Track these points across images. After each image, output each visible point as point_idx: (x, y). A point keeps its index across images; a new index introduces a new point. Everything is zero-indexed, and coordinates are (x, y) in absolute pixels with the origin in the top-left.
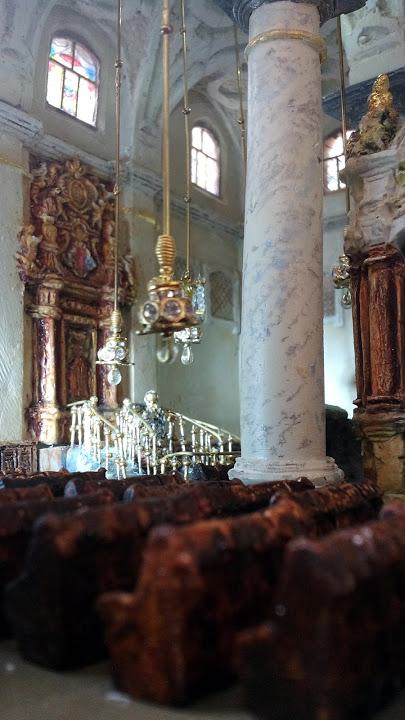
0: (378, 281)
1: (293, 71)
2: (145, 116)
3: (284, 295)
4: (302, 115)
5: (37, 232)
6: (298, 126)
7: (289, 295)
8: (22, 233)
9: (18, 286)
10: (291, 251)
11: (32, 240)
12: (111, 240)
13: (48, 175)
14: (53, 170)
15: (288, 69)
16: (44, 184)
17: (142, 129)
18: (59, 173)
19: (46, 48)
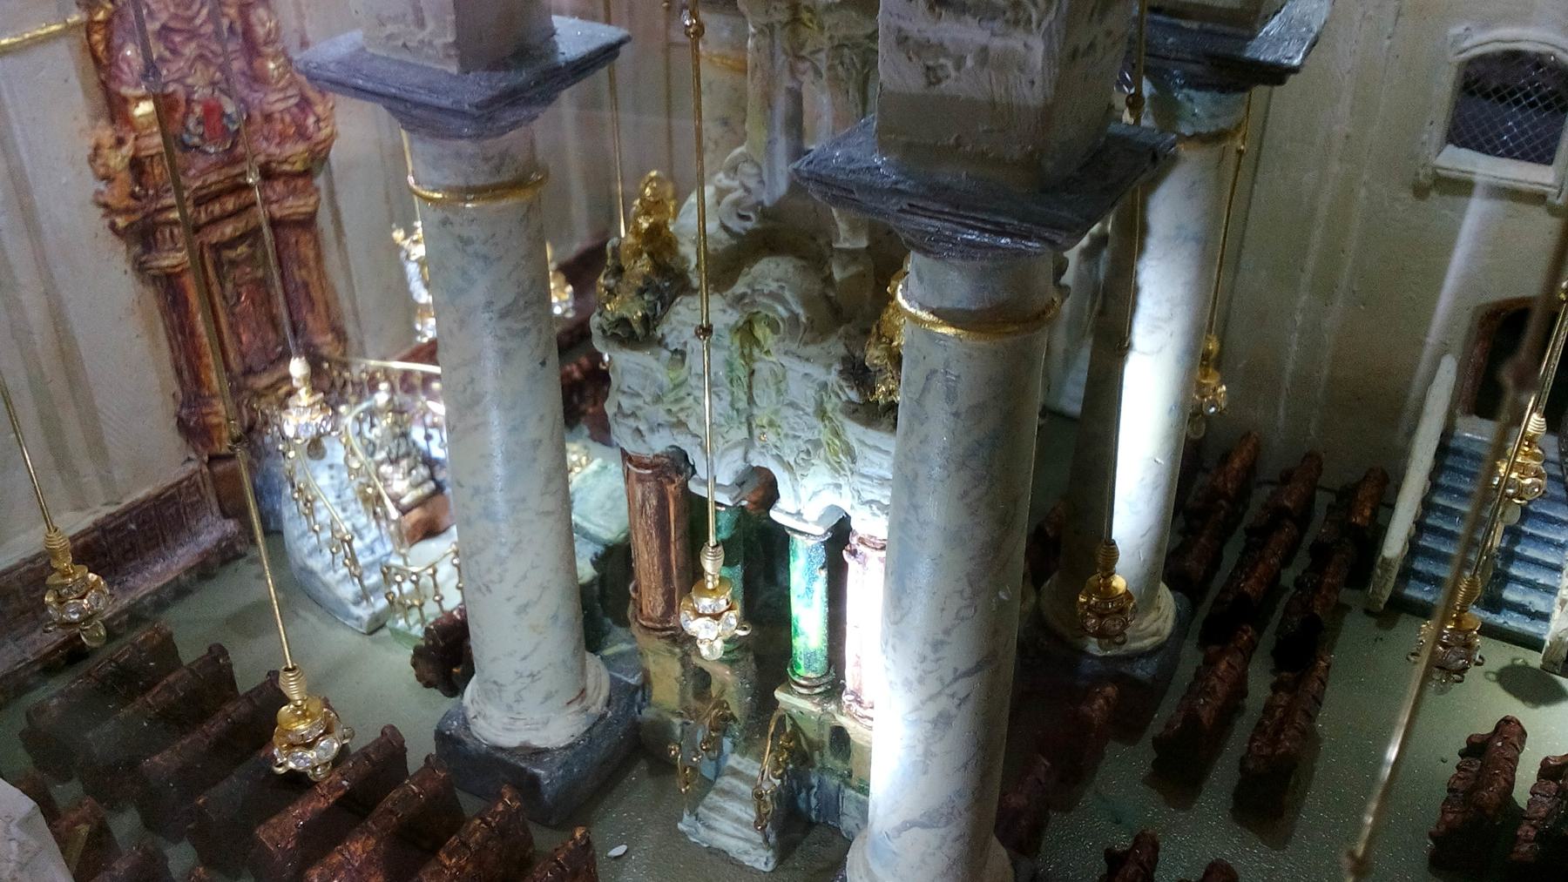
4: (508, 322)
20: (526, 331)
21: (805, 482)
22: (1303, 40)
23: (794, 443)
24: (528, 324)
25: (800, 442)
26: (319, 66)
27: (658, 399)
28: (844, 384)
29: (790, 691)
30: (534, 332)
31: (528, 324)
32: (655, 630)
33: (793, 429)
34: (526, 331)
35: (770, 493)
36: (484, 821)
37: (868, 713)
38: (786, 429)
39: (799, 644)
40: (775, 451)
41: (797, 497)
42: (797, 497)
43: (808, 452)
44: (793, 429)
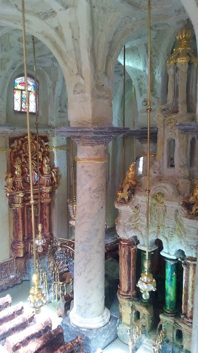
0: (124, 251)
1: (91, 176)
2: (60, 105)
3: (86, 262)
4: (95, 194)
5: (13, 175)
6: (93, 198)
7: (88, 262)
8: (7, 178)
9: (6, 200)
10: (89, 246)
11: (10, 180)
12: (46, 166)
13: (18, 144)
14: (20, 142)
15: (89, 175)
16: (16, 150)
17: (59, 111)
18: (23, 142)
19: (13, 84)
20: (99, 197)
21: (170, 243)
22: (148, 34)
23: (167, 229)
24: (99, 196)
25: (170, 229)
26: (137, 9)
27: (130, 220)
28: (183, 208)
29: (165, 315)
30: (100, 199)
31: (99, 196)
32: (125, 296)
33: (168, 225)
34: (99, 197)
35: (161, 248)
36: (72, 343)
37: (190, 320)
38: (166, 226)
39: (167, 298)
40: (162, 234)
41: (168, 248)
42: (168, 248)
43: (172, 232)
44: (168, 225)
